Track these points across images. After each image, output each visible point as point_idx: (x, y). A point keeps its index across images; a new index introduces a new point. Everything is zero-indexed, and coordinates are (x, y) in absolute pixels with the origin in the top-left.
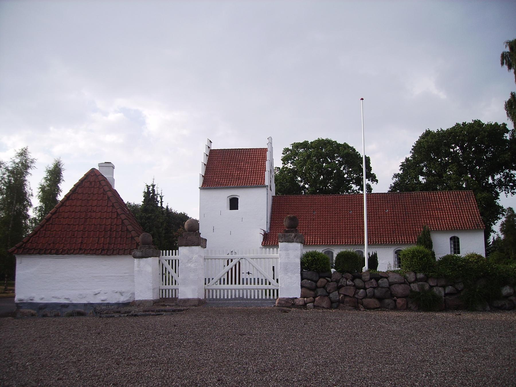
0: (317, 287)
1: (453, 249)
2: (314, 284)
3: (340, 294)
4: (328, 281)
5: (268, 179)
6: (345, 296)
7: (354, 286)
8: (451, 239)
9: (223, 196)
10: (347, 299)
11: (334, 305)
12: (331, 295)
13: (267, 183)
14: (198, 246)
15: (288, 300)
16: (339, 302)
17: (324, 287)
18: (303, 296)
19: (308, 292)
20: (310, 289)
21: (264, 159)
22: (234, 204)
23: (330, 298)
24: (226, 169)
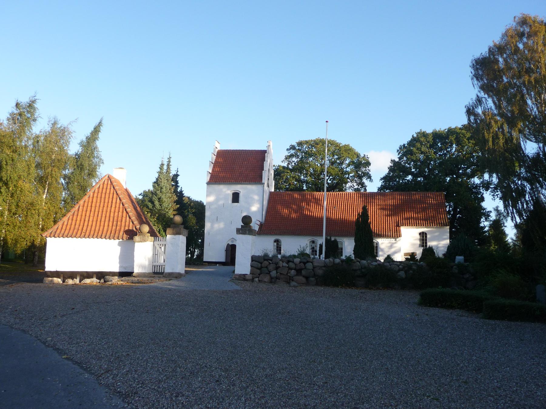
0: (262, 267)
1: (276, 247)
2: (259, 265)
3: (277, 273)
4: (270, 263)
5: (268, 175)
6: (281, 274)
7: (288, 267)
8: (275, 241)
9: (227, 190)
10: (282, 276)
11: (273, 280)
12: (271, 273)
13: (265, 180)
14: (180, 234)
15: (240, 275)
16: (277, 278)
17: (267, 267)
18: (252, 273)
19: (255, 269)
20: (257, 268)
21: (263, 159)
22: (236, 198)
23: (270, 275)
24: (238, 167)
